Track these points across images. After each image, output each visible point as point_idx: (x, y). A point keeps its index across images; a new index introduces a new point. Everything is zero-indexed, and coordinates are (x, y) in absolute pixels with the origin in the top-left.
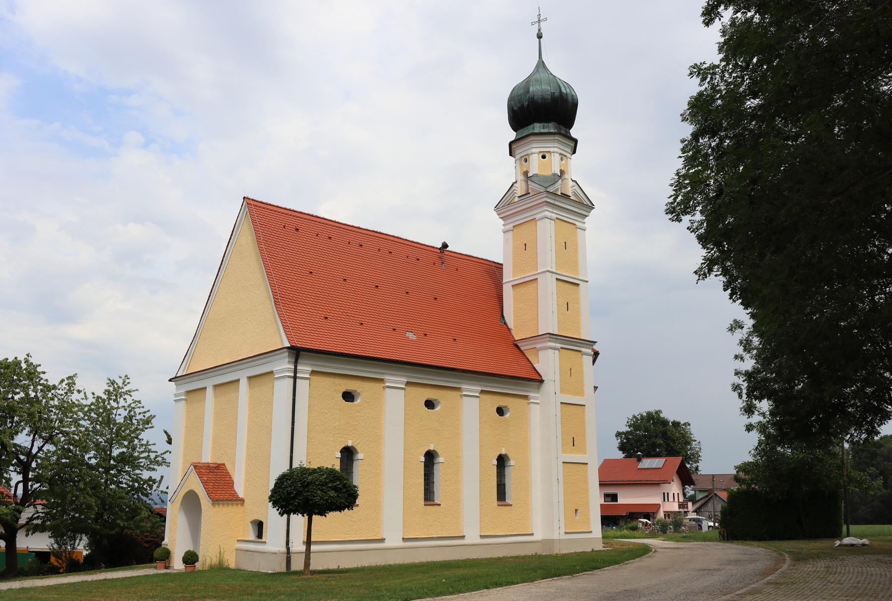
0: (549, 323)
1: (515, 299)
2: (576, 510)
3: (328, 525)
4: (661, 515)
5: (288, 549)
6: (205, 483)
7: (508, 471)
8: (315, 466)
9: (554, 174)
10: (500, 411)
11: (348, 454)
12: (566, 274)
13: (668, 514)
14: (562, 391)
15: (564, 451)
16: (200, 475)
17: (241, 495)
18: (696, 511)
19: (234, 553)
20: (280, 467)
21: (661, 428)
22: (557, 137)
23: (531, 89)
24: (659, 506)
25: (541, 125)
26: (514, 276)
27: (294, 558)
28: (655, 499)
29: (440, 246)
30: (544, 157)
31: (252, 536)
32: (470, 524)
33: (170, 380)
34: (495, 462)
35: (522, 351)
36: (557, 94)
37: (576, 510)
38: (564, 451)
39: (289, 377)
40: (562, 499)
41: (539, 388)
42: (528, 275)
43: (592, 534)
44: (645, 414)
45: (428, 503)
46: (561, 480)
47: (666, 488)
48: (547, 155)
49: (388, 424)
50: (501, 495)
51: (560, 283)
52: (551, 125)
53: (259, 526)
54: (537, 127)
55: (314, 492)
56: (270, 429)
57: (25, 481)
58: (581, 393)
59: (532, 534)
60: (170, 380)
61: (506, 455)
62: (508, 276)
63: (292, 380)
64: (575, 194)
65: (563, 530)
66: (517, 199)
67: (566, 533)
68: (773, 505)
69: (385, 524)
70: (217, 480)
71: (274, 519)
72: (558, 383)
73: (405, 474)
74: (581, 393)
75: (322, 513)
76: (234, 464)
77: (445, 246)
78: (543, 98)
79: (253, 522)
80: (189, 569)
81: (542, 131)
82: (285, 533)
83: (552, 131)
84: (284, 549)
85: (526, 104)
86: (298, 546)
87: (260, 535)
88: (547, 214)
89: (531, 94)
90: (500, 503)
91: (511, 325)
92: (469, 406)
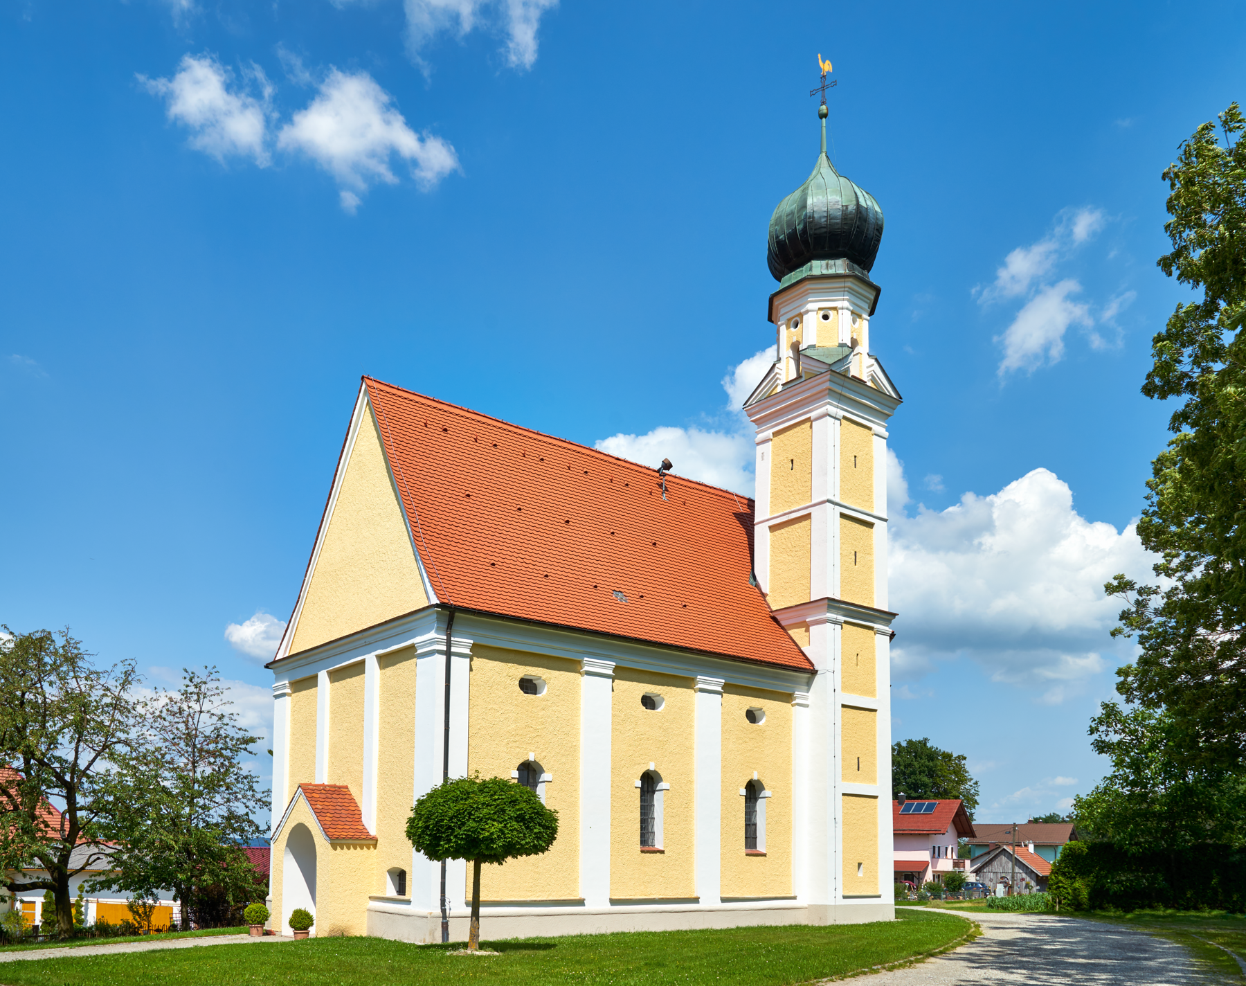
0: (828, 582)
1: (773, 547)
2: (860, 865)
3: (502, 878)
4: (929, 877)
5: (444, 911)
6: (319, 813)
7: (760, 805)
8: (487, 776)
9: (842, 345)
10: (752, 716)
11: (530, 771)
12: (856, 505)
13: (937, 875)
14: (845, 687)
15: (844, 778)
16: (312, 801)
17: (373, 832)
18: (977, 872)
19: (366, 914)
20: (428, 780)
21: (924, 761)
22: (849, 283)
23: (809, 202)
24: (925, 865)
25: (824, 262)
26: (772, 512)
27: (452, 924)
28: (924, 856)
29: (657, 466)
30: (826, 317)
31: (391, 892)
32: (707, 884)
33: (267, 667)
34: (744, 792)
35: (782, 628)
36: (852, 207)
37: (860, 865)
38: (844, 778)
39: (440, 652)
40: (840, 848)
41: (809, 684)
42: (796, 506)
43: (881, 904)
44: (904, 744)
45: (646, 848)
46: (840, 820)
47: (940, 841)
48: (832, 314)
49: (584, 730)
50: (751, 839)
51: (847, 522)
52: (839, 262)
53: (400, 878)
54: (818, 267)
55: (483, 822)
56: (411, 731)
57: (72, 807)
58: (871, 692)
59: (794, 898)
60: (267, 667)
61: (758, 781)
62: (762, 513)
63: (444, 658)
64: (873, 380)
65: (840, 893)
66: (779, 389)
67: (844, 897)
68: (1122, 865)
69: (585, 882)
70: (336, 810)
71: (422, 868)
72: (838, 675)
73: (613, 807)
74: (871, 692)
75: (498, 858)
76: (361, 786)
77: (667, 465)
78: (829, 217)
79: (391, 872)
80: (300, 937)
81: (825, 272)
82: (439, 891)
83: (841, 271)
84: (438, 912)
85: (799, 227)
86: (459, 906)
87: (401, 890)
88: (832, 410)
89: (809, 209)
90: (750, 851)
91: (766, 588)
92: (705, 710)
